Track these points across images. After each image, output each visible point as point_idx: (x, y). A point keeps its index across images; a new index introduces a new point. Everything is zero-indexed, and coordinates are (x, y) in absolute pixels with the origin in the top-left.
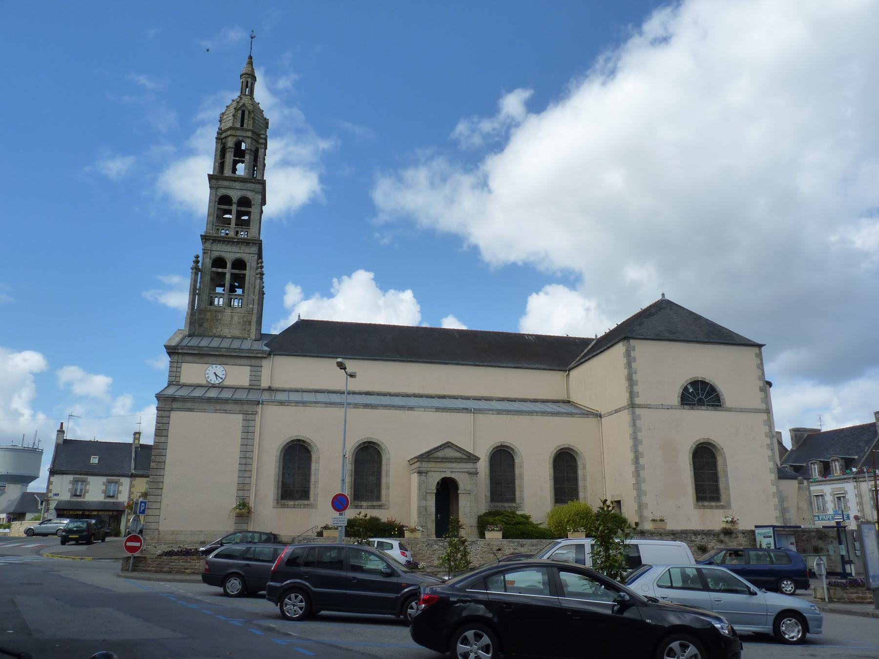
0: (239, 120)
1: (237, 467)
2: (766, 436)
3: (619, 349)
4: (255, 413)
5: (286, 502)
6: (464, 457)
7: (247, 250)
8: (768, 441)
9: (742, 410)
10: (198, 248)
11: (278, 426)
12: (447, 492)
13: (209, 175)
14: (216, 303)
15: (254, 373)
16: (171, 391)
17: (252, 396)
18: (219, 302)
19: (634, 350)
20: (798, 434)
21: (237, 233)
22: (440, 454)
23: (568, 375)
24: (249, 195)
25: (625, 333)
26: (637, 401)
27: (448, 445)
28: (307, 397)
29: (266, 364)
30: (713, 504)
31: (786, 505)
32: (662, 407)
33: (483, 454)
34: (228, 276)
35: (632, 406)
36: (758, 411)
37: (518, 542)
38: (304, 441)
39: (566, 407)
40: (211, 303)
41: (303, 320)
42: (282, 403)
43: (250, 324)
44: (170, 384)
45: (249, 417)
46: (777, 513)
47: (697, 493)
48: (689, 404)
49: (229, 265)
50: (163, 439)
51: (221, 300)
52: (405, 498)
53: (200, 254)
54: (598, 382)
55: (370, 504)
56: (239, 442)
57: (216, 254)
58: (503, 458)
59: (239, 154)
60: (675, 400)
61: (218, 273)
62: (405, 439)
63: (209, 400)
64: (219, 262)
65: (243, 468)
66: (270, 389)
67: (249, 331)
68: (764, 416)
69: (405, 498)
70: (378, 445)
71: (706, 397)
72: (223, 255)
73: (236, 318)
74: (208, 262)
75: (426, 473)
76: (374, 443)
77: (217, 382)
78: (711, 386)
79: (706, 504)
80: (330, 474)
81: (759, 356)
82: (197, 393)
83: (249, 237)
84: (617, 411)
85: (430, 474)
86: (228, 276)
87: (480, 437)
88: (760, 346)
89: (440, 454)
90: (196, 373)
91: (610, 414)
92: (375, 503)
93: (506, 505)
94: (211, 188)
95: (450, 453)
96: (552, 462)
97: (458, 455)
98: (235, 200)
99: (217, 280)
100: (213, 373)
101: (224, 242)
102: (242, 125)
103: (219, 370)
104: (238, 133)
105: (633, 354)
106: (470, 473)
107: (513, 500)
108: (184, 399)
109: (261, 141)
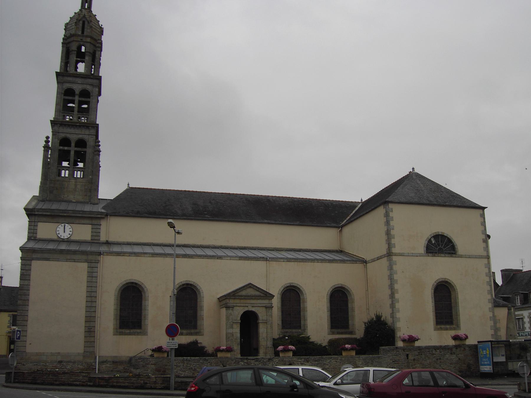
0: (80, 29)
1: (84, 304)
2: (487, 276)
3: (381, 211)
4: (98, 262)
5: (123, 330)
7: (87, 132)
8: (487, 279)
9: (470, 257)
10: (48, 131)
11: (115, 272)
12: (249, 322)
13: (56, 72)
14: (63, 175)
15: (94, 230)
16: (31, 245)
17: (94, 249)
18: (65, 174)
20: (507, 274)
21: (79, 118)
22: (244, 293)
23: (341, 231)
24: (89, 88)
25: (383, 199)
27: (250, 286)
28: (137, 249)
29: (103, 223)
30: (448, 327)
31: (498, 325)
33: (276, 290)
34: (72, 153)
35: (389, 254)
36: (480, 257)
37: (305, 359)
38: (136, 284)
39: (341, 255)
40: (60, 174)
42: (118, 254)
44: (29, 239)
45: (93, 265)
46: (492, 332)
47: (436, 319)
48: (432, 253)
49: (73, 144)
50: (26, 282)
51: (67, 172)
52: (216, 329)
53: (50, 135)
54: (363, 236)
55: (188, 331)
58: (292, 296)
59: (81, 57)
60: (422, 250)
61: (64, 150)
62: (215, 281)
63: (62, 252)
64: (65, 142)
66: (107, 243)
68: (486, 261)
69: (216, 329)
70: (195, 287)
71: (444, 247)
72: (68, 136)
73: (79, 187)
76: (191, 285)
78: (448, 238)
79: (443, 326)
80: (159, 309)
81: (483, 216)
82: (51, 246)
83: (88, 122)
84: (378, 258)
85: (235, 308)
86: (72, 153)
87: (274, 279)
88: (483, 208)
89: (244, 293)
90: (46, 230)
91: (373, 260)
92: (193, 331)
93: (294, 330)
94: (58, 83)
96: (329, 297)
97: (257, 293)
98: (77, 92)
99: (63, 156)
100: (64, 231)
101: (69, 125)
102: (83, 32)
105: (391, 214)
106: (266, 307)
107: (300, 327)
108: (42, 251)
109: (97, 45)
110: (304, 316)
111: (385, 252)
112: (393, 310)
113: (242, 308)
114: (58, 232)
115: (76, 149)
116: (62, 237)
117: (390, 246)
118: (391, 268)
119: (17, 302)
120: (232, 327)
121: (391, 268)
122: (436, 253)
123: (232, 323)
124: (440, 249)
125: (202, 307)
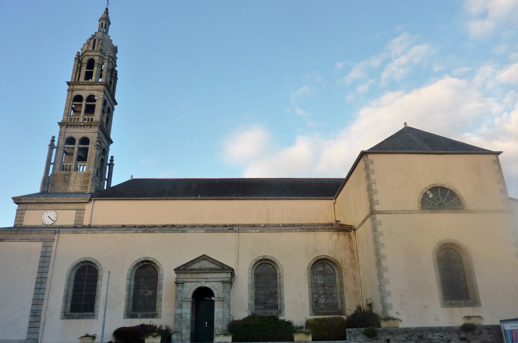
0: (91, 45)
6: (218, 267)
10: (56, 131)
11: (70, 251)
15: (78, 215)
19: (372, 163)
22: (196, 266)
26: (377, 208)
27: (204, 258)
32: (403, 212)
34: (76, 150)
35: (372, 213)
41: (135, 179)
43: (88, 182)
45: (47, 244)
49: (77, 142)
56: (37, 264)
57: (68, 135)
64: (71, 141)
65: (39, 286)
67: (87, 187)
69: (171, 311)
71: (446, 202)
73: (78, 179)
74: (63, 141)
75: (183, 283)
77: (50, 223)
78: (451, 191)
81: (497, 162)
85: (186, 284)
89: (196, 266)
91: (360, 225)
92: (150, 313)
95: (205, 264)
97: (213, 266)
98: (85, 97)
102: (94, 48)
103: (53, 214)
104: (90, 54)
110: (280, 294)
111: (367, 212)
112: (380, 282)
113: (194, 284)
114: (43, 219)
115: (81, 146)
116: (47, 224)
117: (372, 203)
118: (375, 229)
119: (379, 325)
120: (181, 307)
121: (375, 229)
122: (436, 209)
123: (180, 302)
124: (440, 203)
125: (161, 285)
